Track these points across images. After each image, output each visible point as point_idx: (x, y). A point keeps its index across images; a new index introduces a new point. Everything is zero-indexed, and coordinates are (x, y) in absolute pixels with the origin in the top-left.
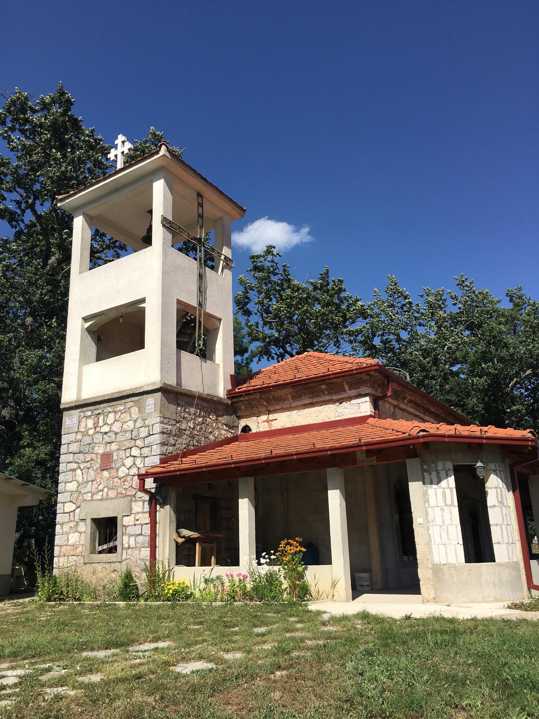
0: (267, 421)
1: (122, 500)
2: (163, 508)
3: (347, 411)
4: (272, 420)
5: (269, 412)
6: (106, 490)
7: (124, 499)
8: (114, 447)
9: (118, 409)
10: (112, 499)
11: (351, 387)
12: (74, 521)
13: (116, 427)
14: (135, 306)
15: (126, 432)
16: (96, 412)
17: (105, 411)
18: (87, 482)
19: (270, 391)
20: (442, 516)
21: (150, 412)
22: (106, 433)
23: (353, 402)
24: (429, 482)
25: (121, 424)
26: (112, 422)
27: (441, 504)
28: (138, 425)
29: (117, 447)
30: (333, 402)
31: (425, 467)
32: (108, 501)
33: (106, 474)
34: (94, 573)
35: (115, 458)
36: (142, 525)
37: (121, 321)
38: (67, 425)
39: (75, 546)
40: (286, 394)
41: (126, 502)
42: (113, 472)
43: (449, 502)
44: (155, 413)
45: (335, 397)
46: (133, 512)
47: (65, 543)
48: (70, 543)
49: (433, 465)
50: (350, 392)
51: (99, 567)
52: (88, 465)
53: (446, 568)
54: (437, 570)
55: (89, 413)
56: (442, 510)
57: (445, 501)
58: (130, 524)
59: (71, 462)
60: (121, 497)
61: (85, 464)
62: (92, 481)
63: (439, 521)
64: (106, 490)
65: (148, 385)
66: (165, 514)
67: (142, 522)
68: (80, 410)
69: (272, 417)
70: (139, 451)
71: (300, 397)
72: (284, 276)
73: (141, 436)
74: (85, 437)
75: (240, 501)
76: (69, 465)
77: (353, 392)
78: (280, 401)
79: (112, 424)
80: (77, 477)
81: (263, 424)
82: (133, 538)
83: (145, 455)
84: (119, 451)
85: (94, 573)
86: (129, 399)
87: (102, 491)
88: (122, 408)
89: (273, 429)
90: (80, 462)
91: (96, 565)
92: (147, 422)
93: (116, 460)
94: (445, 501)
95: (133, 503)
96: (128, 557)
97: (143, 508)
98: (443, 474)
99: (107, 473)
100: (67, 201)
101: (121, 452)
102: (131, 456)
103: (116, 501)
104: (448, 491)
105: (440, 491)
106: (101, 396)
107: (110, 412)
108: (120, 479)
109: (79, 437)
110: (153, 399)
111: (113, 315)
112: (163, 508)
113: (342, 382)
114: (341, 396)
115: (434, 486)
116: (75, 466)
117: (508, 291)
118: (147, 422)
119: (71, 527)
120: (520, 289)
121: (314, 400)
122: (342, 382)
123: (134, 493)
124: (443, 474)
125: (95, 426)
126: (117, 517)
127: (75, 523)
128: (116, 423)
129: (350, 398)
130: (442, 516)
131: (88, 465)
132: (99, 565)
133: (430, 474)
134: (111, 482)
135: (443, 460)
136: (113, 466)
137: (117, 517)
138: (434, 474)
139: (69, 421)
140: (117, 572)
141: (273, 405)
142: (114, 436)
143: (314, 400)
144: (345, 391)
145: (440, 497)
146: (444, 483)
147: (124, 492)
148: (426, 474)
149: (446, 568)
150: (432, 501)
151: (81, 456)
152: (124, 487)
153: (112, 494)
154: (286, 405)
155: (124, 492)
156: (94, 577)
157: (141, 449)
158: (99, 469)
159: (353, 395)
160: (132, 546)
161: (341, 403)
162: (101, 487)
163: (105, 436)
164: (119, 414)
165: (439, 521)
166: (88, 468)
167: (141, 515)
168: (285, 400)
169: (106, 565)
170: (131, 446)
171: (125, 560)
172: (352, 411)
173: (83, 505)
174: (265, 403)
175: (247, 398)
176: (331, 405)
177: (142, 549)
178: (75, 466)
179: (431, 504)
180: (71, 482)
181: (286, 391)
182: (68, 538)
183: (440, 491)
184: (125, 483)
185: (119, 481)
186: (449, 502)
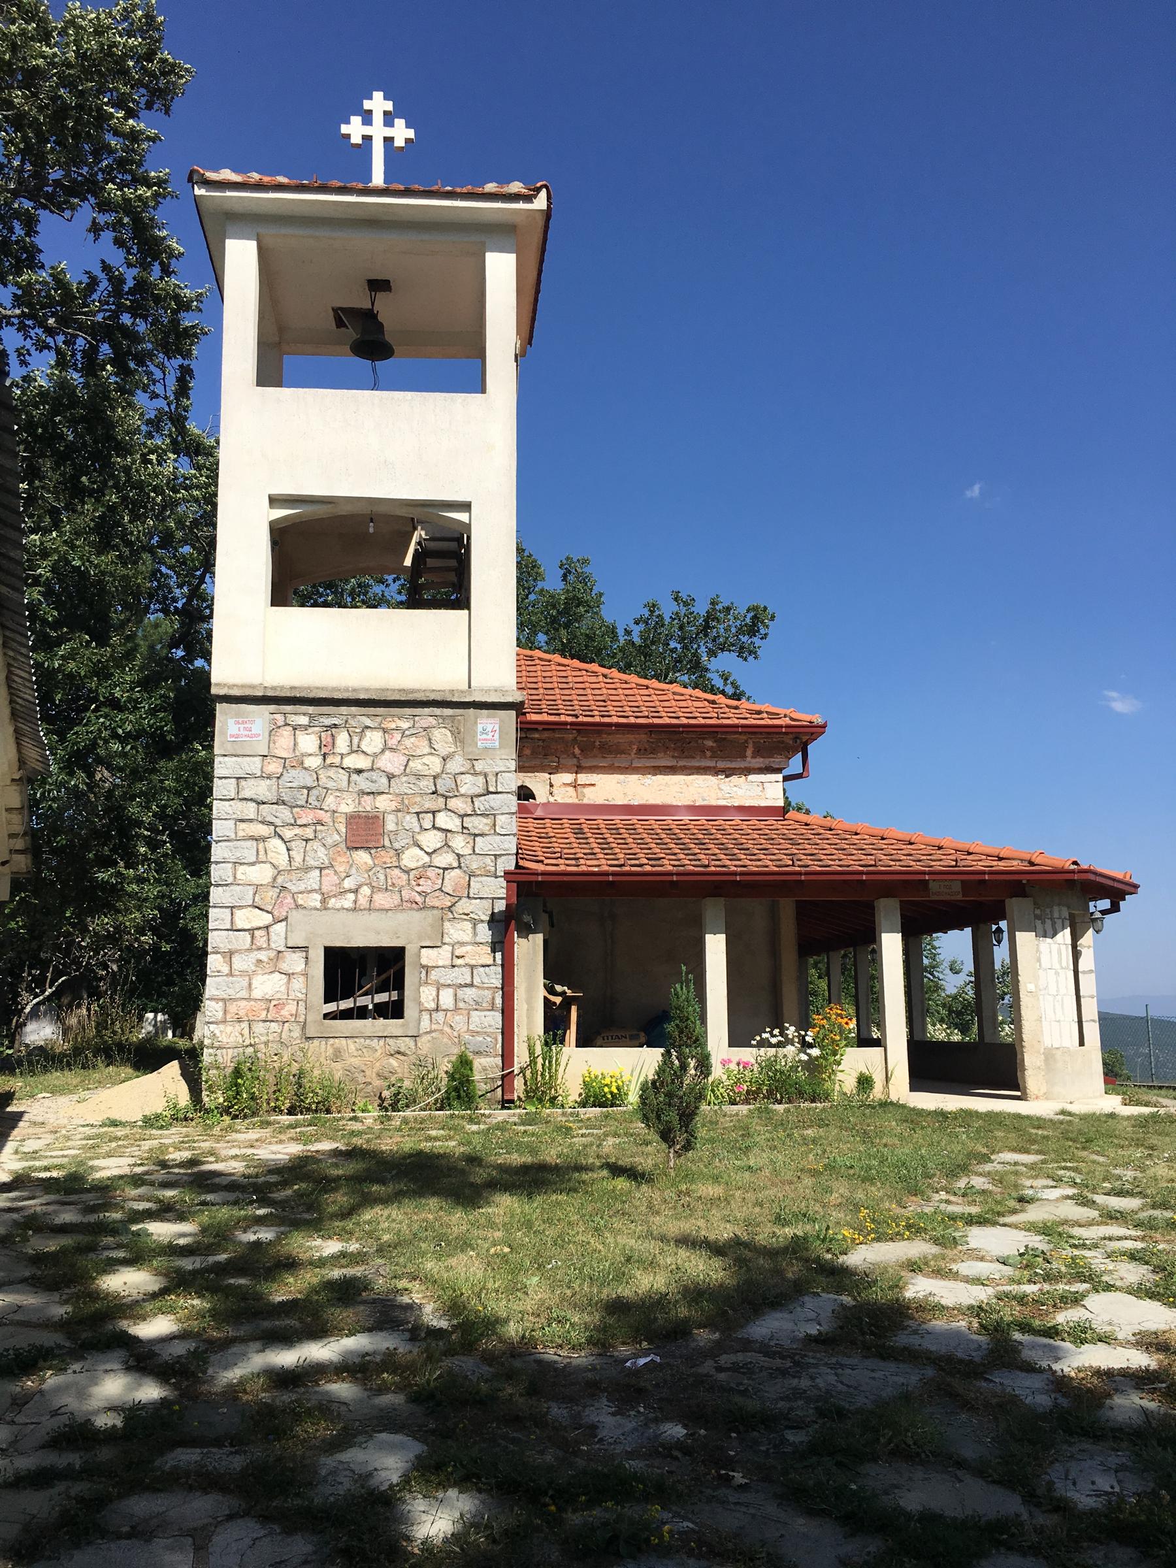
0: (575, 785)
1: (417, 915)
2: (527, 937)
3: (740, 792)
4: (584, 785)
5: (579, 769)
6: (366, 890)
7: (424, 913)
8: (383, 803)
9: (393, 726)
10: (387, 910)
11: (758, 753)
12: (269, 948)
13: (391, 762)
14: (430, 510)
15: (419, 776)
16: (328, 721)
17: (352, 722)
18: (308, 869)
19: (599, 733)
20: (1057, 982)
21: (489, 745)
22: (359, 772)
23: (751, 777)
24: (1042, 933)
25: (404, 759)
26: (378, 750)
27: (1057, 966)
28: (455, 766)
29: (393, 805)
30: (716, 772)
31: (1038, 912)
32: (374, 915)
33: (362, 857)
34: (337, 1055)
35: (390, 826)
36: (472, 967)
37: (371, 530)
38: (232, 736)
39: (274, 1003)
40: (631, 743)
41: (430, 920)
42: (388, 857)
43: (1064, 964)
44: (503, 751)
45: (721, 764)
46: (446, 940)
47: (244, 994)
48: (257, 994)
49: (1048, 911)
50: (754, 760)
51: (352, 1046)
52: (309, 832)
53: (1059, 1053)
54: (1049, 1056)
55: (304, 720)
56: (1057, 973)
57: (1060, 962)
58: (440, 964)
59: (251, 821)
60: (411, 909)
61: (297, 831)
62: (321, 869)
63: (1053, 990)
64: (366, 890)
65: (488, 691)
66: (529, 951)
67: (473, 962)
68: (272, 708)
69: (583, 778)
70: (458, 821)
71: (653, 751)
72: (173, 407)
73: (462, 790)
74: (293, 772)
75: (709, 938)
76: (242, 826)
77: (759, 762)
78: (610, 752)
79: (375, 755)
80: (270, 854)
81: (563, 789)
82: (451, 991)
83: (477, 832)
84: (400, 814)
85: (337, 1055)
86: (427, 711)
87: (356, 891)
88: (405, 725)
89: (586, 801)
90: (278, 822)
91: (343, 1041)
92: (479, 766)
93: (396, 833)
94: (1060, 962)
95: (447, 924)
96: (434, 1027)
97: (475, 934)
98: (1059, 922)
99: (368, 856)
100: (228, 194)
101: (408, 817)
102: (434, 827)
103: (401, 917)
104: (1063, 948)
105: (1055, 947)
106: (347, 690)
107: (368, 727)
108: (407, 872)
109: (274, 767)
110: (497, 720)
111: (344, 510)
112: (527, 937)
113: (746, 741)
114: (733, 765)
115: (1048, 940)
116: (264, 830)
117: (567, 559)
118: (479, 766)
119: (260, 961)
120: (585, 562)
121: (681, 763)
122: (746, 741)
123: (449, 904)
124: (1059, 922)
125: (324, 750)
126: (402, 949)
127: (272, 954)
128: (387, 752)
129: (747, 771)
130: (1057, 982)
131: (309, 832)
132: (350, 1041)
133: (1043, 923)
134: (382, 877)
135: (1059, 905)
136: (387, 843)
137: (402, 949)
138: (1049, 922)
139: (230, 725)
140: (404, 1054)
141: (595, 756)
142: (384, 780)
143: (681, 763)
144: (744, 757)
145: (1055, 953)
146: (1059, 936)
147: (419, 899)
148: (1038, 922)
149: (1059, 1053)
150: (1045, 962)
151: (284, 813)
152: (419, 889)
153: (381, 900)
154: (622, 761)
155: (419, 899)
156: (338, 1066)
157: (462, 816)
158: (343, 845)
159: (757, 766)
160: (444, 1007)
161: (727, 777)
162: (348, 884)
163: (354, 777)
164: (398, 736)
165: (1053, 990)
166: (307, 840)
167: (469, 948)
168: (623, 752)
169: (374, 1043)
170: (434, 807)
171: (427, 1033)
172: (748, 793)
173: (295, 916)
174: (577, 751)
175: (546, 735)
176: (710, 777)
177: (474, 1013)
178: (264, 830)
179: (1044, 965)
180: (253, 864)
181: (631, 737)
182: (250, 985)
183: (1055, 947)
184: (421, 881)
185: (405, 877)
186: (1064, 964)
